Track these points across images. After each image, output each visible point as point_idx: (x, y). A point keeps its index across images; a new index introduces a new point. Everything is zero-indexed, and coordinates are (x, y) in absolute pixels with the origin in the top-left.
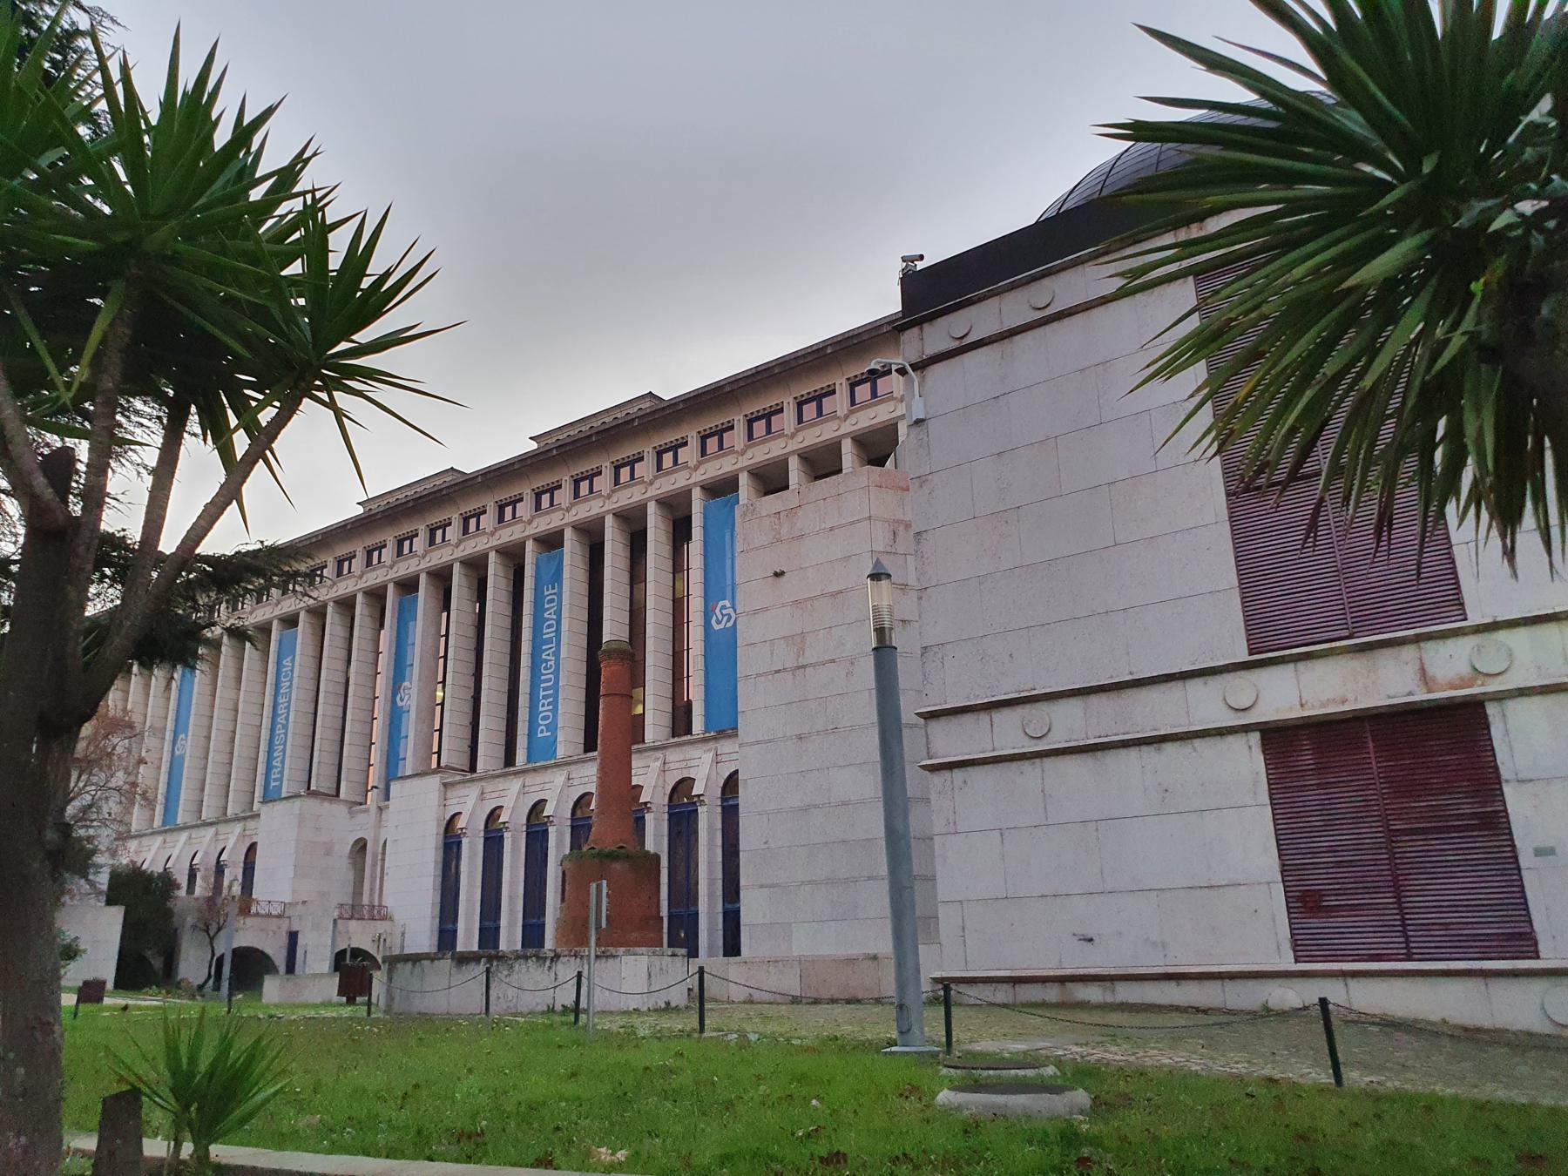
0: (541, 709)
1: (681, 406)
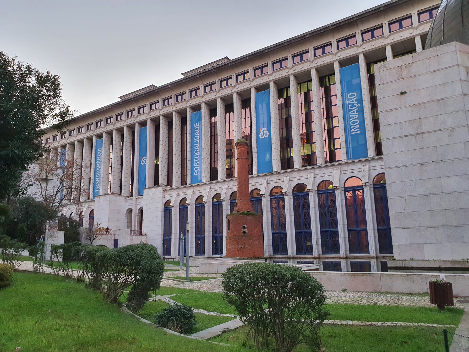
0: (195, 166)
1: (247, 58)
